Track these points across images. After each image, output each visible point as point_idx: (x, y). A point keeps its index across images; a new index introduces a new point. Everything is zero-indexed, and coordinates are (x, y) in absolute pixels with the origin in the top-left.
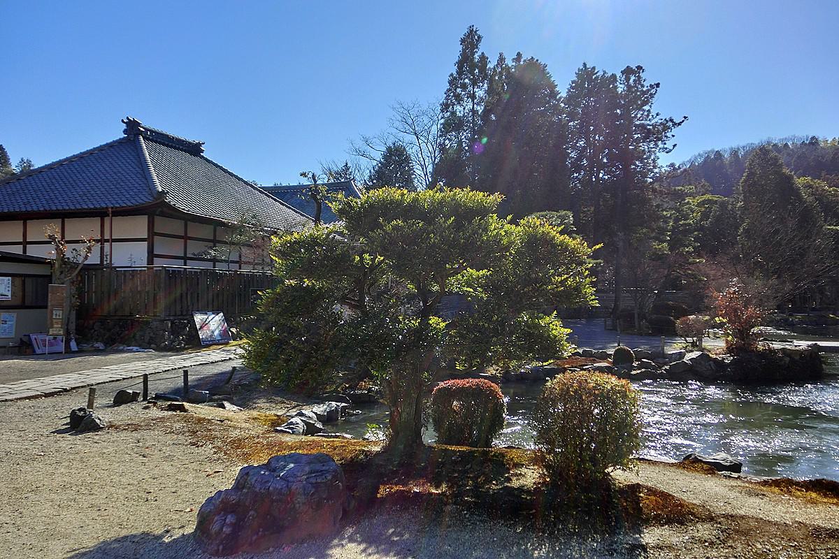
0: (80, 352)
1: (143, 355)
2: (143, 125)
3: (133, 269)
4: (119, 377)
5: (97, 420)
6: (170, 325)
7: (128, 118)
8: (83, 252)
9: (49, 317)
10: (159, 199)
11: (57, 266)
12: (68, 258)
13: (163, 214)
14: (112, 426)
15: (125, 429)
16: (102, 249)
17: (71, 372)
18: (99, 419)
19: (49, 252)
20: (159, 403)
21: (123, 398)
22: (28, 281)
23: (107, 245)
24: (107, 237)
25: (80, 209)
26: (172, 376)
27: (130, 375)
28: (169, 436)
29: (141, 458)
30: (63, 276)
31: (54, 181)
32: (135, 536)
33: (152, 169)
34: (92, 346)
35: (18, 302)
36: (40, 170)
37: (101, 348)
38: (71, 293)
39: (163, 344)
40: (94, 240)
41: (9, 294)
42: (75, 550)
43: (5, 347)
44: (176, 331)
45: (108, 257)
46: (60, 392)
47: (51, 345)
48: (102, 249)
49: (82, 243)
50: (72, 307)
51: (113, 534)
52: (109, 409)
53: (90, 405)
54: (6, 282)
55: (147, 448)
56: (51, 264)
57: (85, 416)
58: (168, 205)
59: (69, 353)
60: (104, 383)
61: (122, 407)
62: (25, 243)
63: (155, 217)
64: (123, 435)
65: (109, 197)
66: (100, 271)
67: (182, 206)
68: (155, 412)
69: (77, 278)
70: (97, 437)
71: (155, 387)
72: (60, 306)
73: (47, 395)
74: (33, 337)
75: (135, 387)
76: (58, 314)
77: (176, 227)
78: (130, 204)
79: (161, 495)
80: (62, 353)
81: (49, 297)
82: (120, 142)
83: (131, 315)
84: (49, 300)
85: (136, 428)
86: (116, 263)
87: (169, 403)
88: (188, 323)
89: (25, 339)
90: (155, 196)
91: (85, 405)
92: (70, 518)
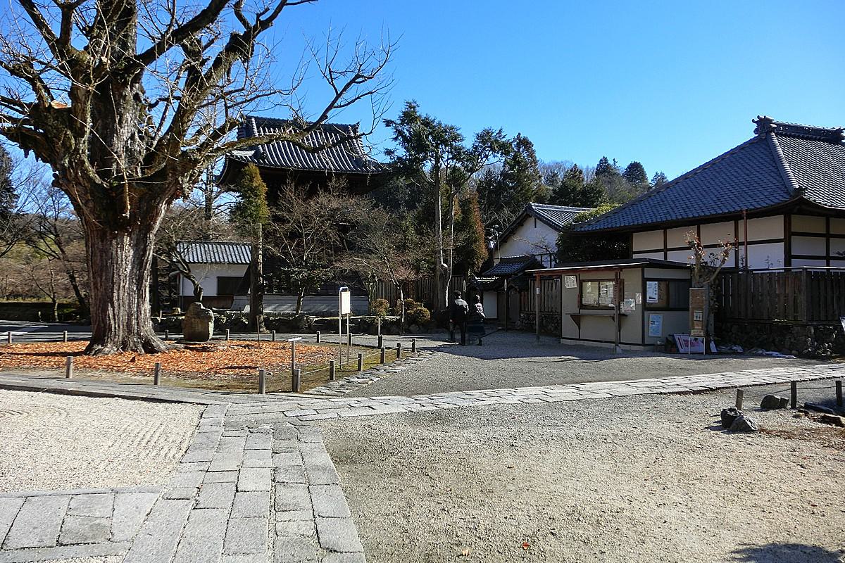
0: (720, 354)
1: (785, 361)
2: (775, 121)
3: (770, 271)
4: (763, 382)
5: (748, 422)
6: (813, 331)
7: (758, 117)
8: (721, 255)
9: (690, 319)
10: (797, 196)
11: (696, 270)
12: (706, 263)
13: (801, 212)
14: (763, 430)
15: (778, 436)
16: (737, 253)
17: (714, 373)
18: (750, 421)
19: (688, 258)
20: (810, 413)
21: (770, 404)
22: (672, 286)
23: (742, 248)
24: (741, 239)
25: (753, 209)
26: (821, 386)
27: (773, 380)
28: (828, 450)
29: (799, 467)
30: (702, 280)
31: (689, 189)
32: (806, 547)
33: (787, 165)
34: (731, 349)
35: (663, 304)
36: (676, 181)
37: (739, 351)
38: (709, 296)
39: (806, 351)
40: (731, 244)
41: (656, 297)
42: (745, 544)
43: (654, 345)
44: (820, 338)
45: (744, 260)
46: (706, 390)
47: (692, 345)
48: (737, 253)
49: (715, 248)
50: (711, 309)
51: (782, 538)
52: (757, 413)
53: (739, 404)
54: (653, 286)
55: (805, 458)
56: (691, 269)
57: (736, 417)
58: (807, 202)
59: (709, 354)
60: (748, 386)
61: (771, 413)
62: (666, 250)
63: (793, 216)
64: (777, 441)
65: (743, 199)
66: (736, 274)
67: (825, 202)
68: (806, 422)
69: (714, 282)
70: (750, 439)
71: (804, 396)
72: (700, 308)
73: (695, 392)
74: (677, 337)
75: (783, 393)
76: (698, 316)
77: (818, 225)
78: (765, 205)
79: (828, 510)
80: (702, 353)
81: (690, 300)
82: (751, 142)
83: (769, 319)
84: (690, 302)
85: (789, 436)
86: (753, 265)
87: (822, 415)
88: (835, 329)
89: (670, 339)
90: (792, 194)
91: (733, 405)
92: (735, 513)
